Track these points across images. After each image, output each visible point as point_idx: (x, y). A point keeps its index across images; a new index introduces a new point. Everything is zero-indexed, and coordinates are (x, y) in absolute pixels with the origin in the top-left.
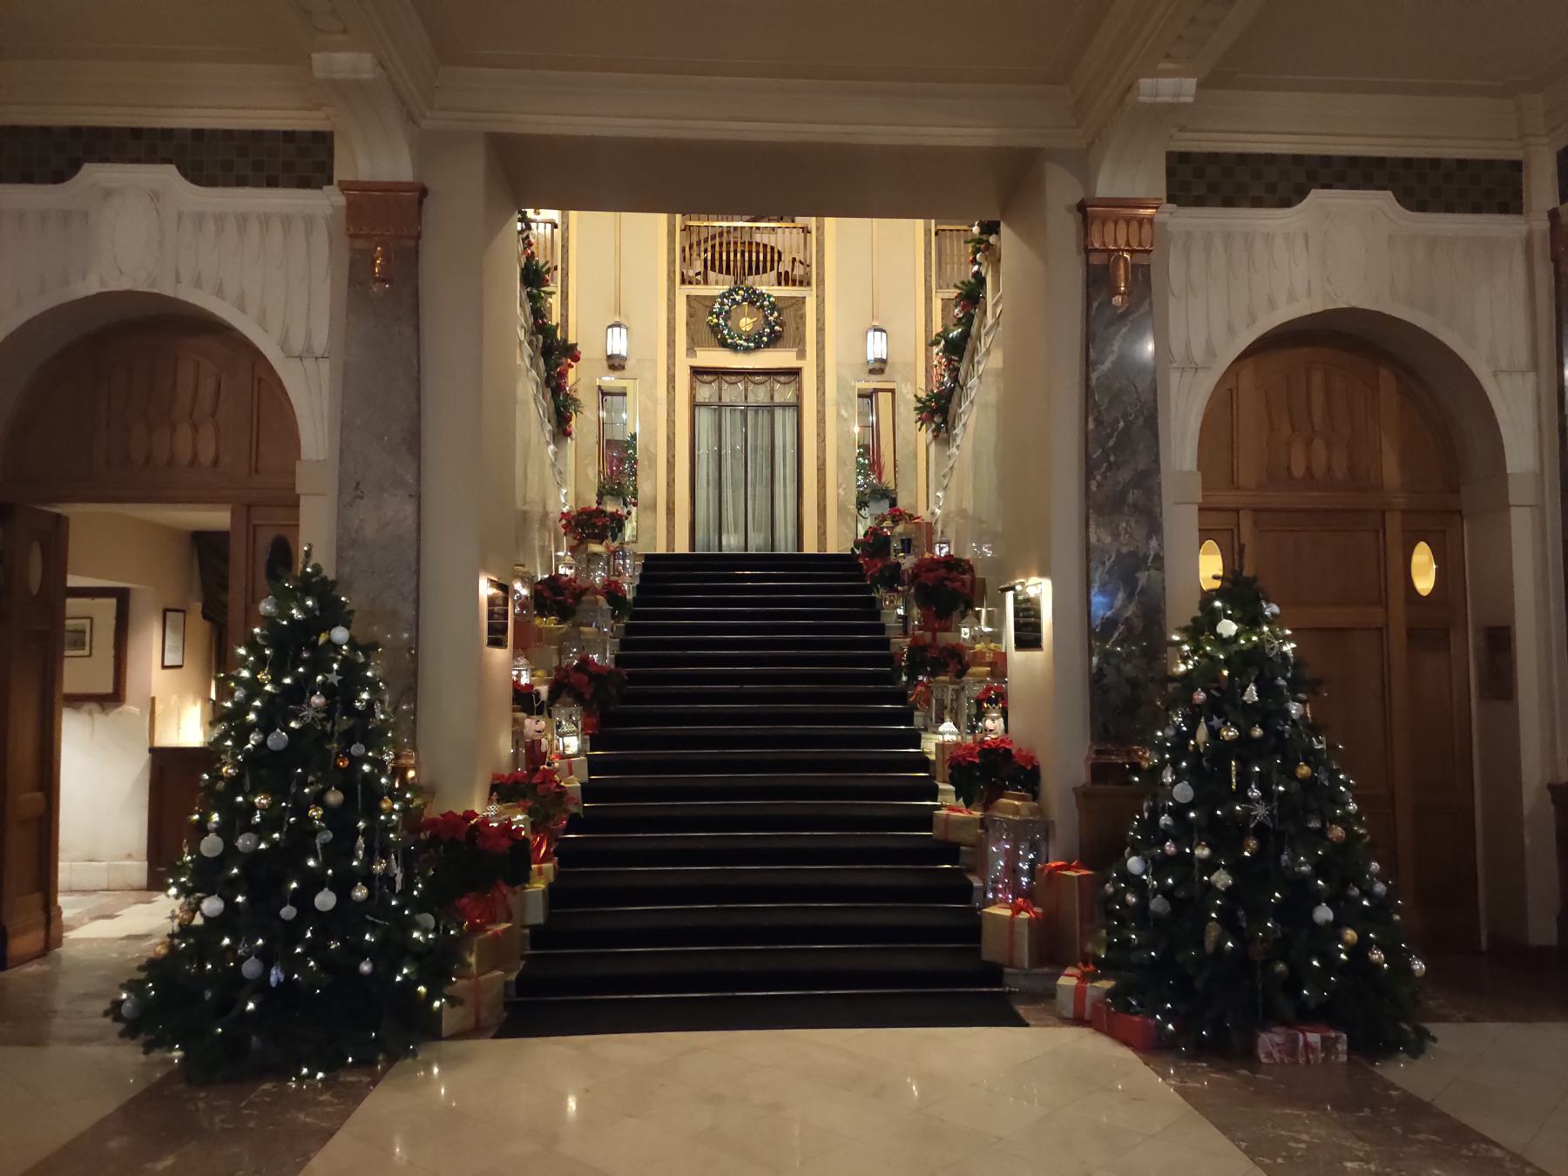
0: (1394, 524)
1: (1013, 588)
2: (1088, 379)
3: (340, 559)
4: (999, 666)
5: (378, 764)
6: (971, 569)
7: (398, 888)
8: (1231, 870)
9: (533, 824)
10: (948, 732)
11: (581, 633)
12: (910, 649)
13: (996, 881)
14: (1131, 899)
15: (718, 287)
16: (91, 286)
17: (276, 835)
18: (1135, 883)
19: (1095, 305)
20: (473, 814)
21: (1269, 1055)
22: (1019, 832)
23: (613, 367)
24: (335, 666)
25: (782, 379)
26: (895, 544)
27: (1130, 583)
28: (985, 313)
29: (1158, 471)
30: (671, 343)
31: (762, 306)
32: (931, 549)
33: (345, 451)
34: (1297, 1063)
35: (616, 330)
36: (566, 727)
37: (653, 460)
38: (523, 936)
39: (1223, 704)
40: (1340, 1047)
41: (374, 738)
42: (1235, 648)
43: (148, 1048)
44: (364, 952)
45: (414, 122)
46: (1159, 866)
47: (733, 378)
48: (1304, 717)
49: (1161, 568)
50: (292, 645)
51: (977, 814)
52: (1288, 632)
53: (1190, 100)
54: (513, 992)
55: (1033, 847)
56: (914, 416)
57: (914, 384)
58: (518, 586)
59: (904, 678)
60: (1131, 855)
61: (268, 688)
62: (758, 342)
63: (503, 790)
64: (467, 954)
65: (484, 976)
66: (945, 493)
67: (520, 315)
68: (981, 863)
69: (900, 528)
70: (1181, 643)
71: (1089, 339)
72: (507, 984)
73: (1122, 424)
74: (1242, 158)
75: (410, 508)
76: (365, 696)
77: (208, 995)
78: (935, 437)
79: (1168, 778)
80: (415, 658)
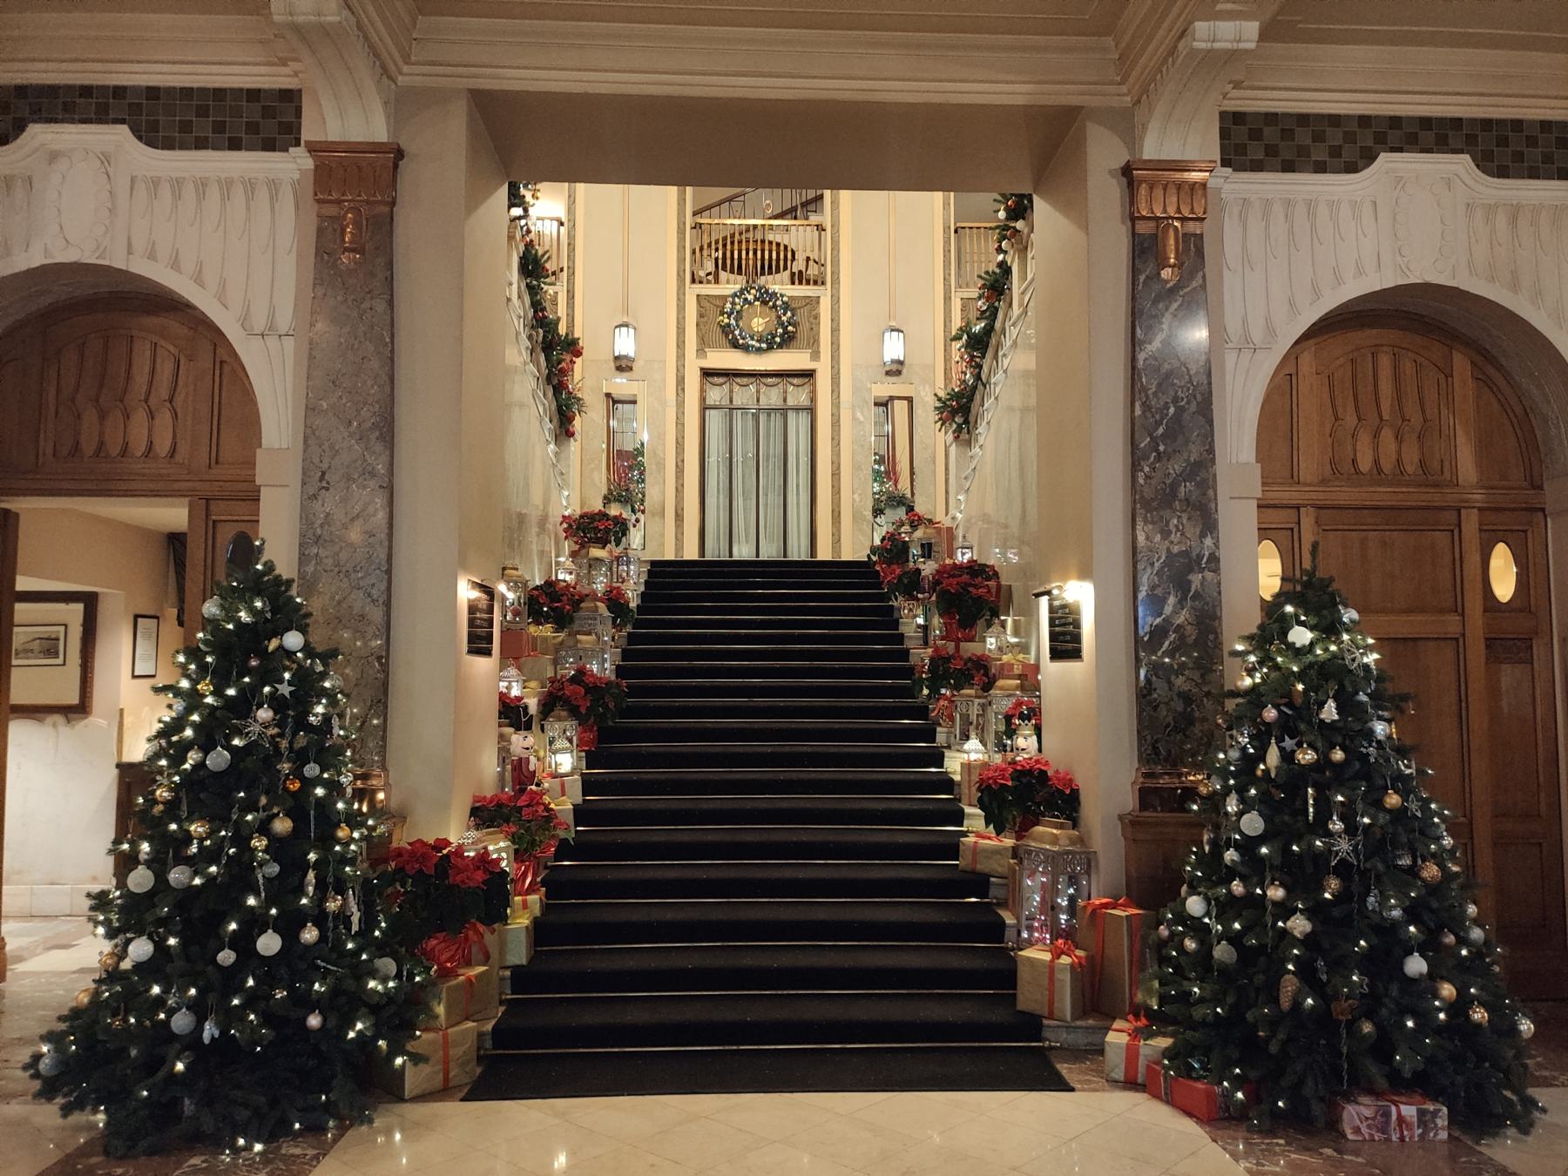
0: (1471, 523)
1: (1048, 593)
2: (1134, 359)
3: (303, 558)
4: (1029, 679)
5: (335, 788)
6: (996, 574)
7: (355, 928)
8: (1310, 913)
9: (516, 851)
10: (974, 751)
11: (578, 641)
12: (932, 659)
13: (1031, 918)
14: (1190, 945)
15: (729, 285)
16: (34, 258)
17: (213, 869)
18: (1196, 927)
19: (1142, 278)
20: (447, 843)
21: (1357, 1131)
22: (1055, 862)
23: (619, 369)
24: (287, 676)
25: (795, 381)
26: (915, 550)
27: (1183, 587)
28: (1010, 305)
29: (1213, 461)
30: (681, 344)
31: (775, 306)
32: (951, 555)
33: (310, 436)
34: (1388, 1140)
35: (624, 330)
36: (561, 743)
37: (661, 466)
38: (502, 979)
39: (1298, 721)
40: (1440, 1122)
41: (328, 756)
42: (1310, 658)
43: (66, 1111)
44: (310, 1003)
45: (390, 78)
46: (1225, 908)
47: (745, 380)
48: (1389, 737)
49: (1216, 571)
50: (234, 656)
51: (1009, 842)
52: (1370, 641)
53: (1252, 45)
54: (488, 1044)
55: (1073, 880)
56: (934, 416)
57: (935, 376)
58: (502, 588)
59: (926, 692)
60: (1190, 894)
61: (209, 700)
62: (771, 343)
63: (485, 815)
64: (434, 1004)
65: (450, 1030)
66: (972, 500)
67: (519, 307)
68: (1013, 898)
69: (919, 533)
70: (1247, 653)
71: (1135, 316)
72: (481, 1035)
73: (1172, 410)
74: (1303, 119)
75: (380, 501)
76: (320, 709)
77: (134, 1053)
78: (957, 438)
79: (1232, 806)
80: (385, 668)
